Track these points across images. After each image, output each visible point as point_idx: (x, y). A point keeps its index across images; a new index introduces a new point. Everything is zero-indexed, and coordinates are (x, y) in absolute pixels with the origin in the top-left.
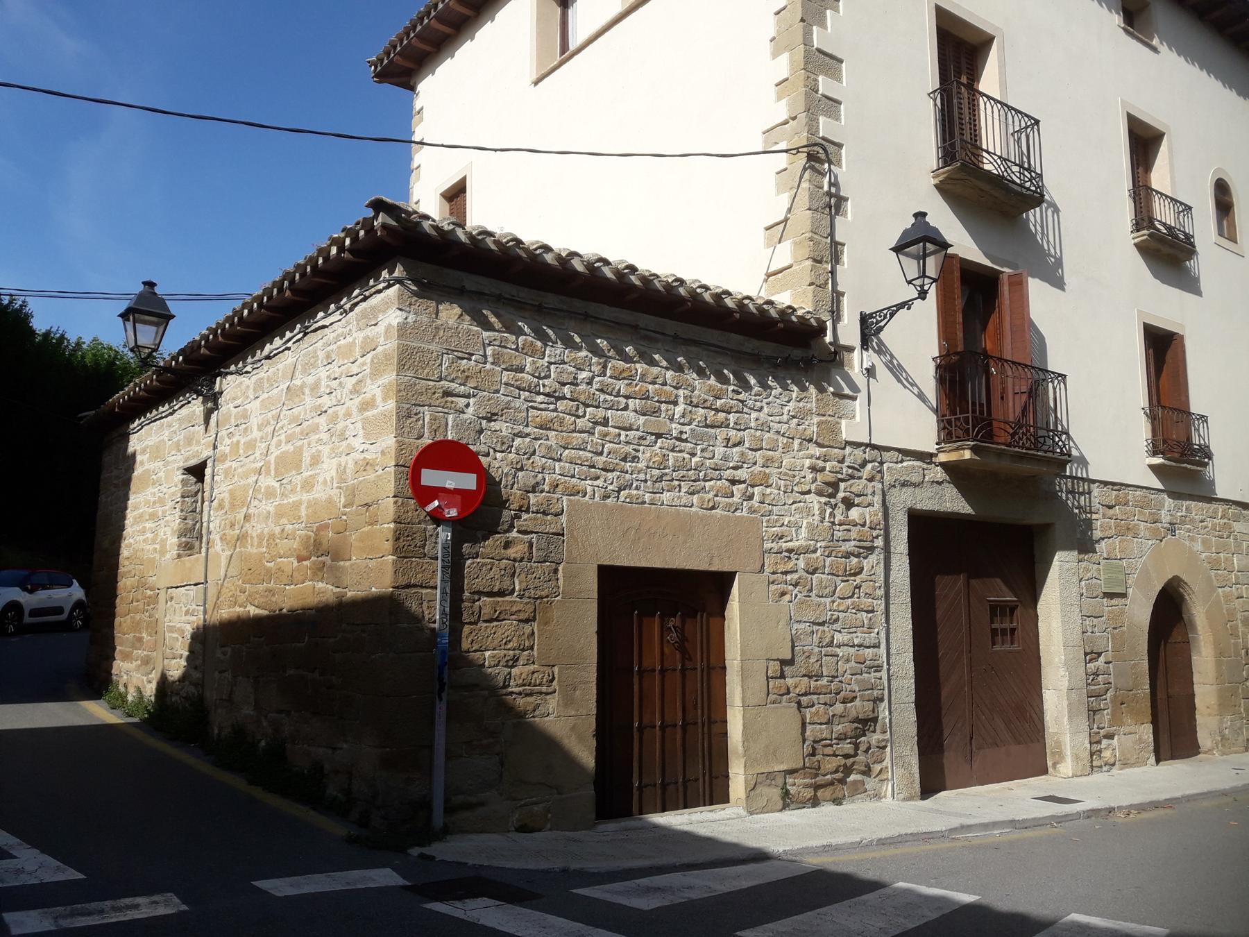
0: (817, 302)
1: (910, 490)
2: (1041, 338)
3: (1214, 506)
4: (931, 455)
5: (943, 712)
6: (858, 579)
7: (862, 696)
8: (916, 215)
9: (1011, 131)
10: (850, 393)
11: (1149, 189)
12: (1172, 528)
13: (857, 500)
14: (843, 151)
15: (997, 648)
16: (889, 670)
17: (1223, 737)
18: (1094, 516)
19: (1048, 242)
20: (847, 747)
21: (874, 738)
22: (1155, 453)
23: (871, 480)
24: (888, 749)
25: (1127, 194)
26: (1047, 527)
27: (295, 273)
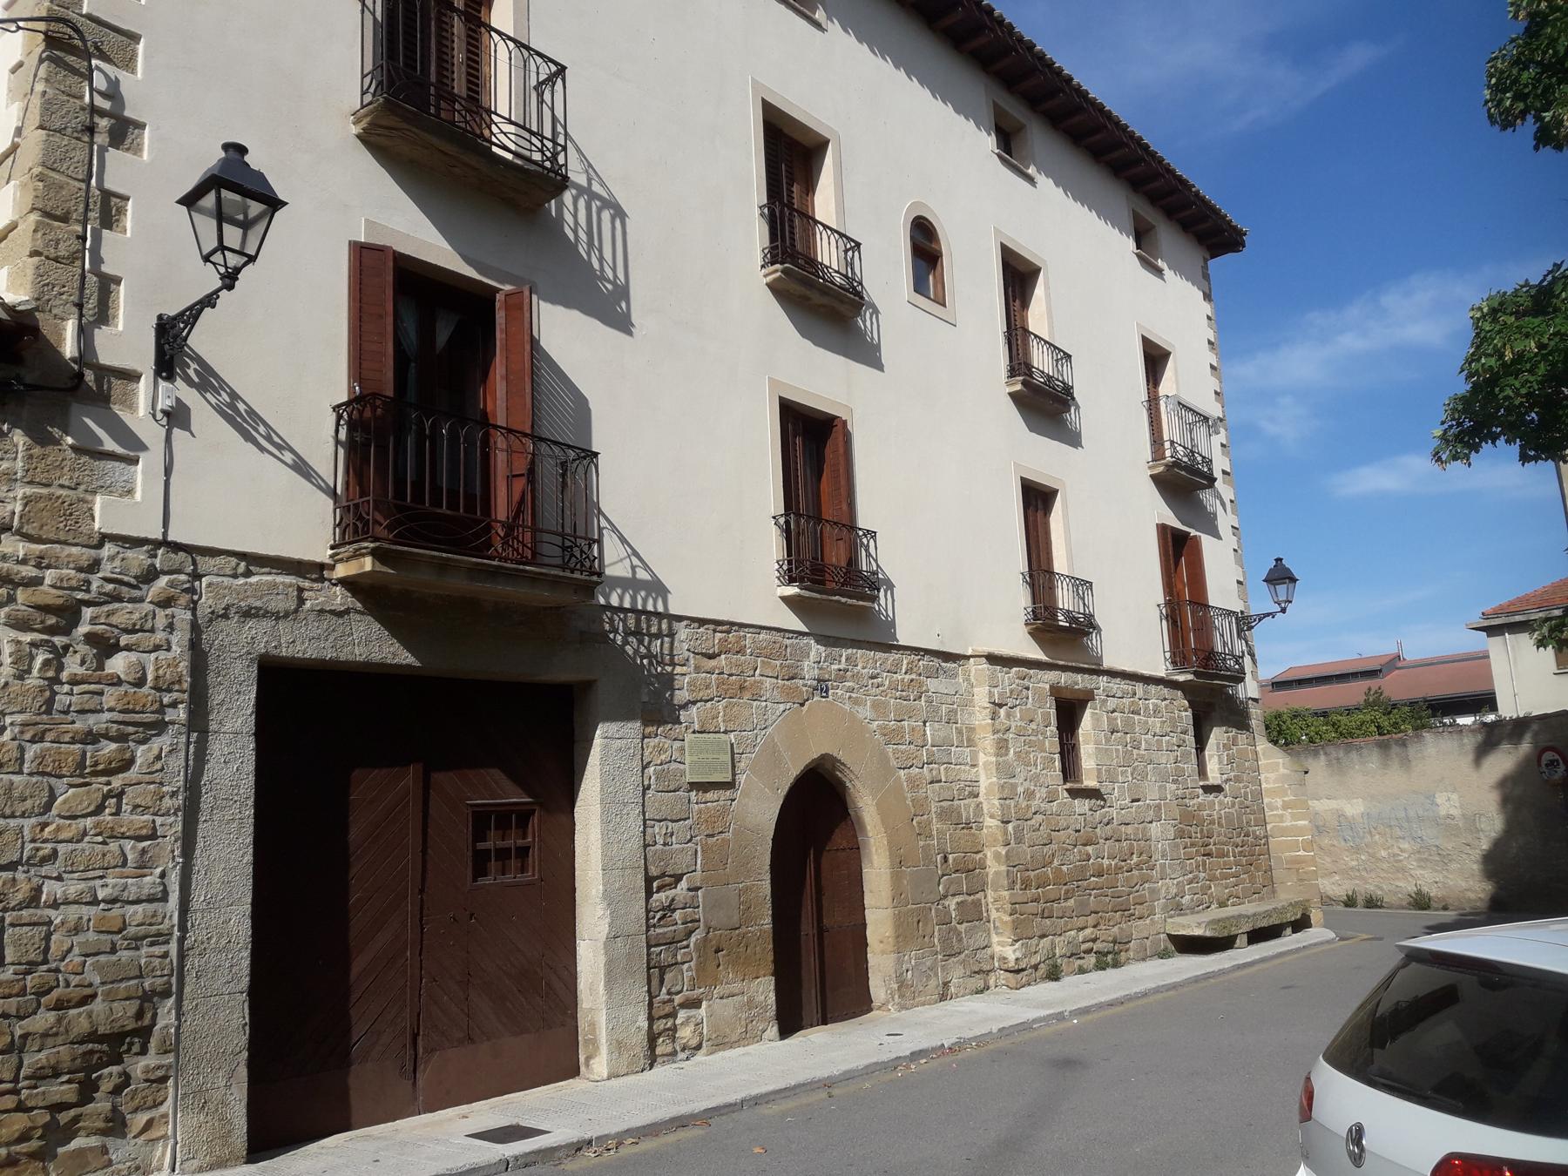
0: (43, 286)
1: (267, 624)
2: (582, 403)
3: (894, 656)
4: (322, 567)
5: (354, 997)
6: (117, 782)
7: (107, 994)
8: (227, 147)
9: (534, 82)
10: (119, 450)
11: (1026, 331)
12: (822, 687)
13: (124, 640)
14: (141, 47)
15: (482, 881)
16: (182, 940)
17: (902, 984)
18: (678, 670)
19: (601, 259)
20: (61, 1090)
21: (139, 1066)
22: (791, 581)
23: (166, 603)
24: (171, 1082)
25: (757, 212)
26: (587, 686)
27: (10, 430)
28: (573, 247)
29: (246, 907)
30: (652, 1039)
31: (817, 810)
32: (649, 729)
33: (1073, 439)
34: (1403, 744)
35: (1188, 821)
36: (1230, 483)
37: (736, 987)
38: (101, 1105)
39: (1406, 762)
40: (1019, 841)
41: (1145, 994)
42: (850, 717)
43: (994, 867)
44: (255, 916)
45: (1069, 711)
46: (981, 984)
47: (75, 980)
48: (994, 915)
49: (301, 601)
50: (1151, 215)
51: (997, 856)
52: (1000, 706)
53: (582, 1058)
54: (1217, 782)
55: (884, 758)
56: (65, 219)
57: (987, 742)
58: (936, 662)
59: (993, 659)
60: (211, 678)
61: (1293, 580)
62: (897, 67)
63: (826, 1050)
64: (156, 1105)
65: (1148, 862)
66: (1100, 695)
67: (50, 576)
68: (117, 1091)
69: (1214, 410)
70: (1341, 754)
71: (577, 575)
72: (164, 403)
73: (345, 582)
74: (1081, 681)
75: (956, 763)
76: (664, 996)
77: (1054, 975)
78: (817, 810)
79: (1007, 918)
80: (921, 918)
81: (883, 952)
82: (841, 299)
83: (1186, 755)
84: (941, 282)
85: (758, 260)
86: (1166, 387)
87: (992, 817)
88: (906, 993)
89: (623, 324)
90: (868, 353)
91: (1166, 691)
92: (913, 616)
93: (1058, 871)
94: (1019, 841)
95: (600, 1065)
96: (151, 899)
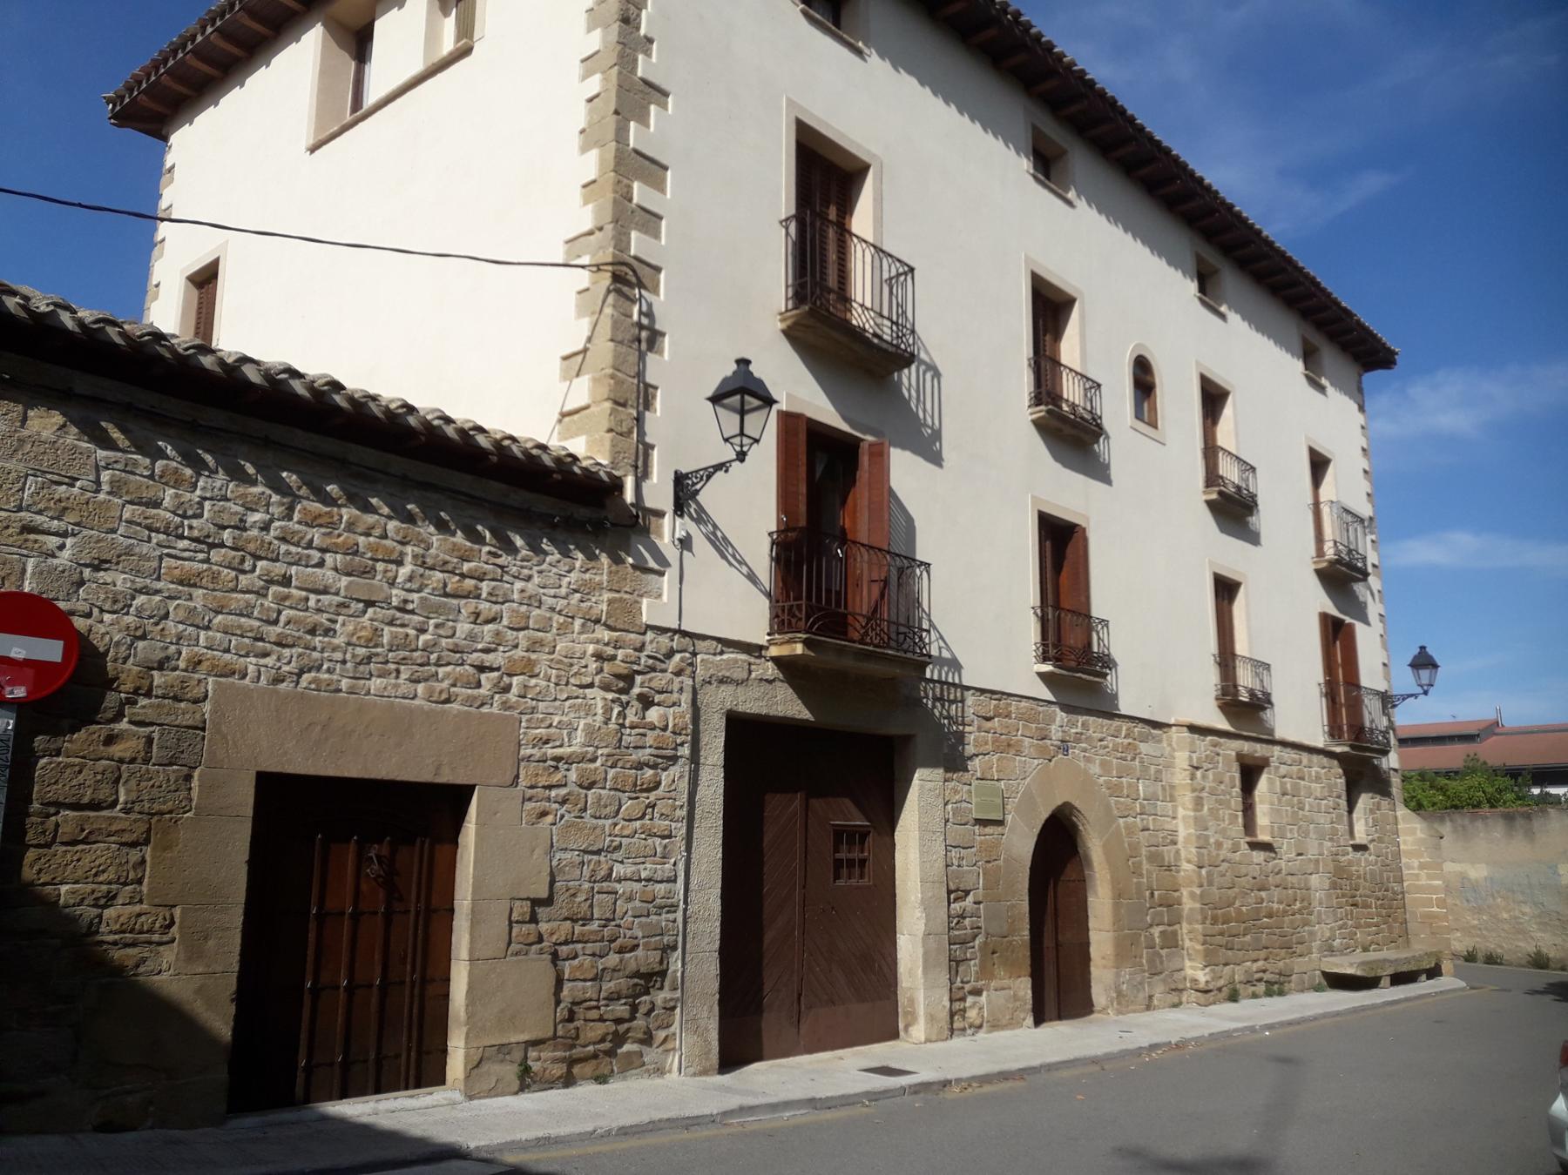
1: (731, 688)
2: (910, 521)
3: (1116, 723)
4: (761, 648)
5: (766, 961)
6: (652, 796)
7: (645, 944)
10: (656, 567)
12: (1064, 746)
13: (657, 698)
14: (662, 276)
16: (685, 910)
17: (1120, 994)
18: (967, 729)
19: (925, 411)
20: (621, 1009)
21: (660, 997)
23: (678, 673)
24: (678, 1010)
26: (907, 739)
28: (908, 402)
29: (717, 891)
30: (952, 1014)
31: (1059, 842)
32: (949, 775)
33: (1253, 538)
34: (1528, 817)
35: (1340, 875)
36: (1379, 576)
37: (1006, 982)
38: (640, 1022)
39: (1530, 835)
40: (1210, 883)
41: (1315, 1018)
42: (1084, 770)
43: (1188, 905)
44: (723, 897)
45: (1250, 773)
46: (1176, 1000)
47: (629, 933)
48: (1187, 943)
49: (750, 672)
50: (1317, 339)
51: (1192, 895)
52: (1197, 768)
53: (901, 1026)
54: (1364, 842)
55: (1108, 808)
56: (624, 405)
57: (1186, 798)
58: (1147, 729)
59: (1193, 729)
60: (702, 727)
61: (1435, 666)
62: (1126, 231)
63: (1062, 1040)
64: (669, 1026)
65: (1307, 908)
66: (1274, 762)
67: (620, 653)
68: (648, 1014)
69: (1366, 510)
70: (1466, 822)
71: (909, 655)
72: (680, 533)
73: (775, 660)
74: (1260, 750)
75: (1166, 815)
76: (958, 984)
77: (1233, 997)
78: (1059, 842)
79: (1199, 947)
80: (1134, 941)
81: (1105, 967)
82: (1086, 430)
83: (1339, 817)
84: (1153, 409)
85: (1027, 404)
86: (1327, 490)
87: (1189, 862)
88: (1121, 1001)
89: (936, 459)
90: (1099, 471)
91: (1325, 761)
92: (1132, 690)
93: (1239, 911)
94: (1210, 883)
95: (919, 1031)
96: (668, 881)
